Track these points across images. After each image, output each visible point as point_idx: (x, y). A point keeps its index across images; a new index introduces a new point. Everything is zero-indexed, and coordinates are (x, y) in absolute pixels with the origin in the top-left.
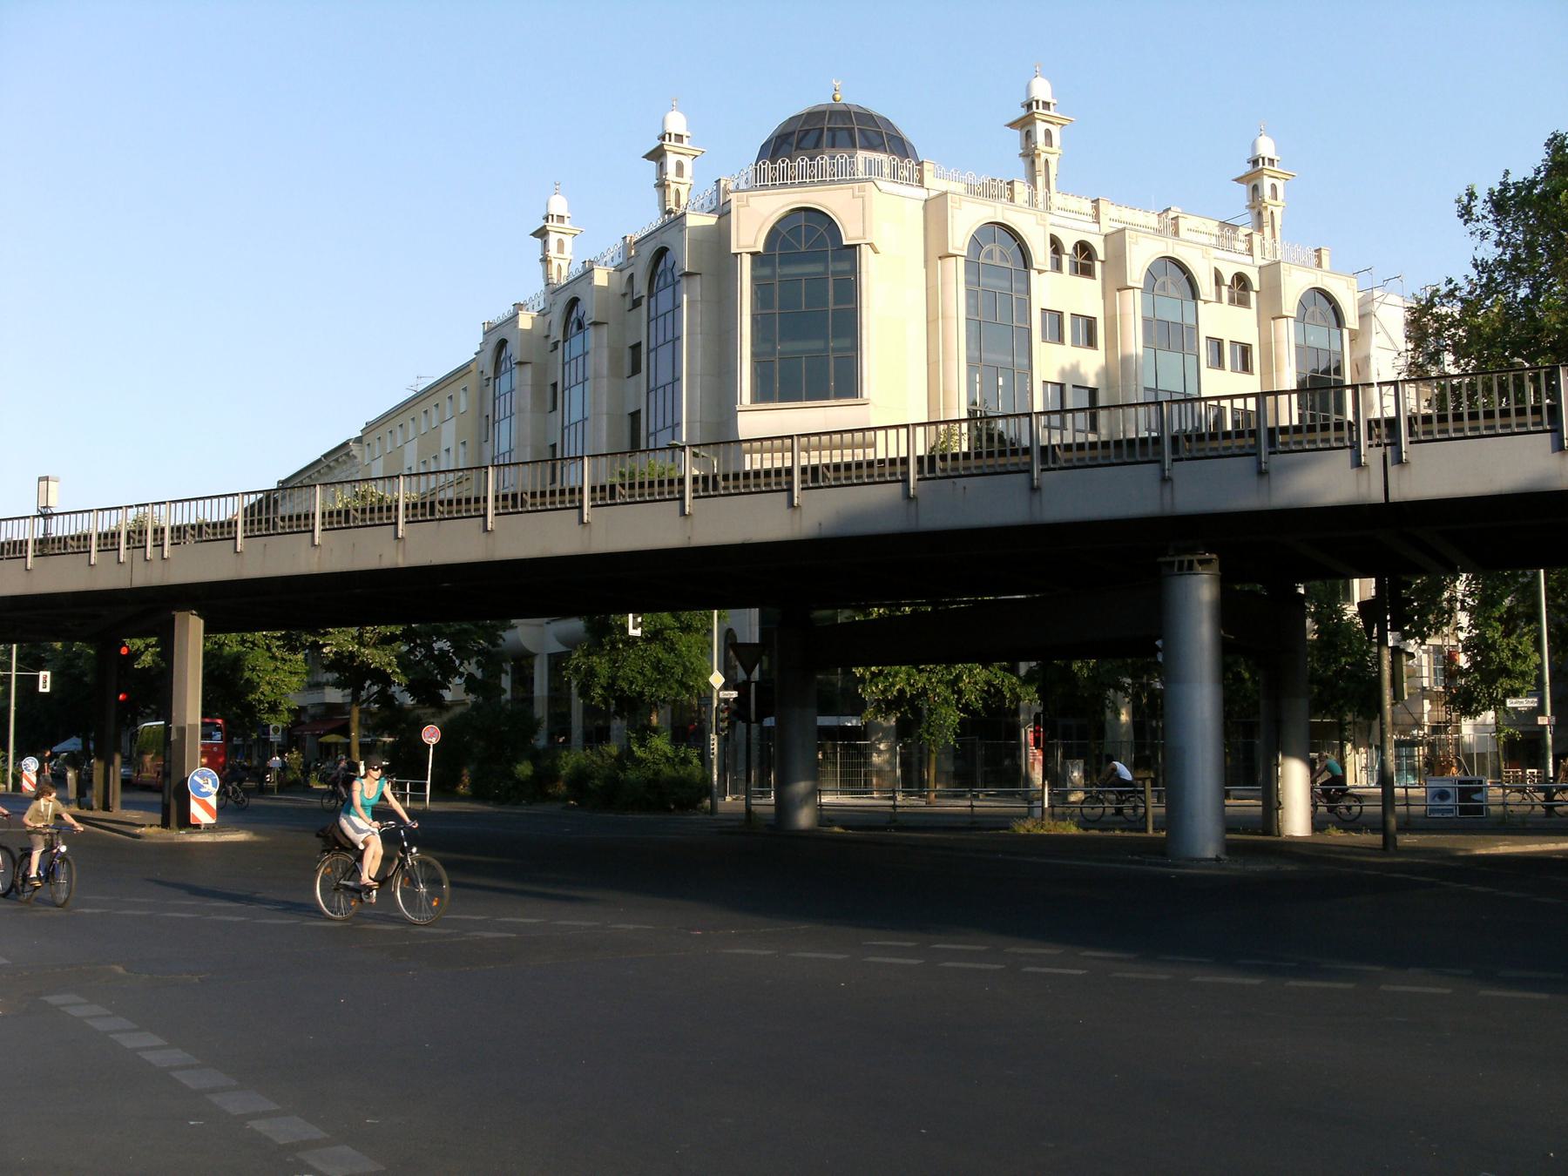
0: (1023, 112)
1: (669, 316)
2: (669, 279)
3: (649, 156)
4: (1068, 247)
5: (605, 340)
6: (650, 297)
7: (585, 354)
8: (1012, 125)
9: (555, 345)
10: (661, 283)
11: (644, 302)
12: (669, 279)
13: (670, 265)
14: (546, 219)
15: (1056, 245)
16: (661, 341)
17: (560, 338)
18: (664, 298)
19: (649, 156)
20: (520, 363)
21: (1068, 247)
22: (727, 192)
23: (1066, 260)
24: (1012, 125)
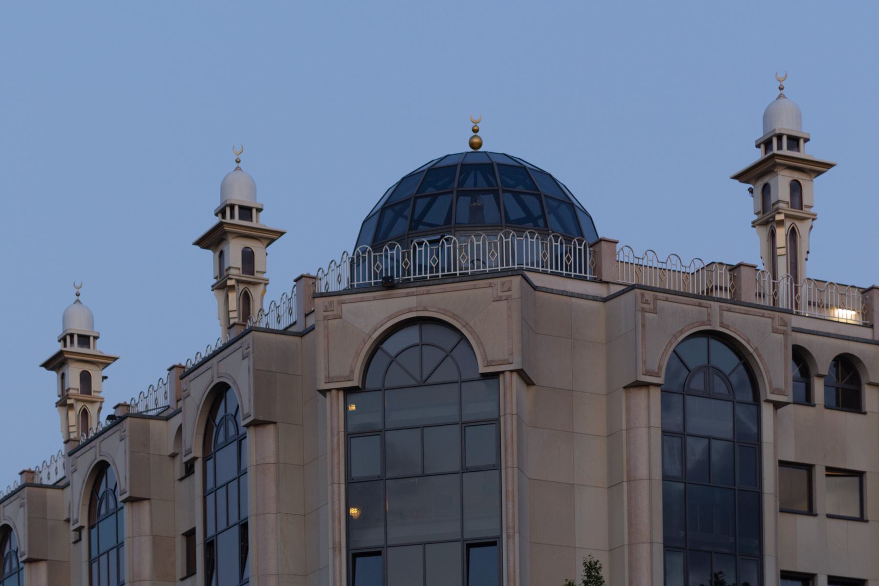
0: (758, 155)
1: (233, 486)
2: (232, 431)
3: (205, 242)
4: (823, 364)
5: (146, 527)
6: (205, 459)
7: (119, 546)
8: (741, 177)
9: (189, 468)
10: (221, 439)
11: (198, 466)
12: (232, 431)
13: (231, 410)
14: (64, 339)
15: (801, 357)
16: (222, 525)
17: (198, 452)
18: (226, 457)
19: (205, 242)
20: (29, 561)
21: (823, 364)
22: (68, 390)
23: (819, 388)
24: (741, 177)
